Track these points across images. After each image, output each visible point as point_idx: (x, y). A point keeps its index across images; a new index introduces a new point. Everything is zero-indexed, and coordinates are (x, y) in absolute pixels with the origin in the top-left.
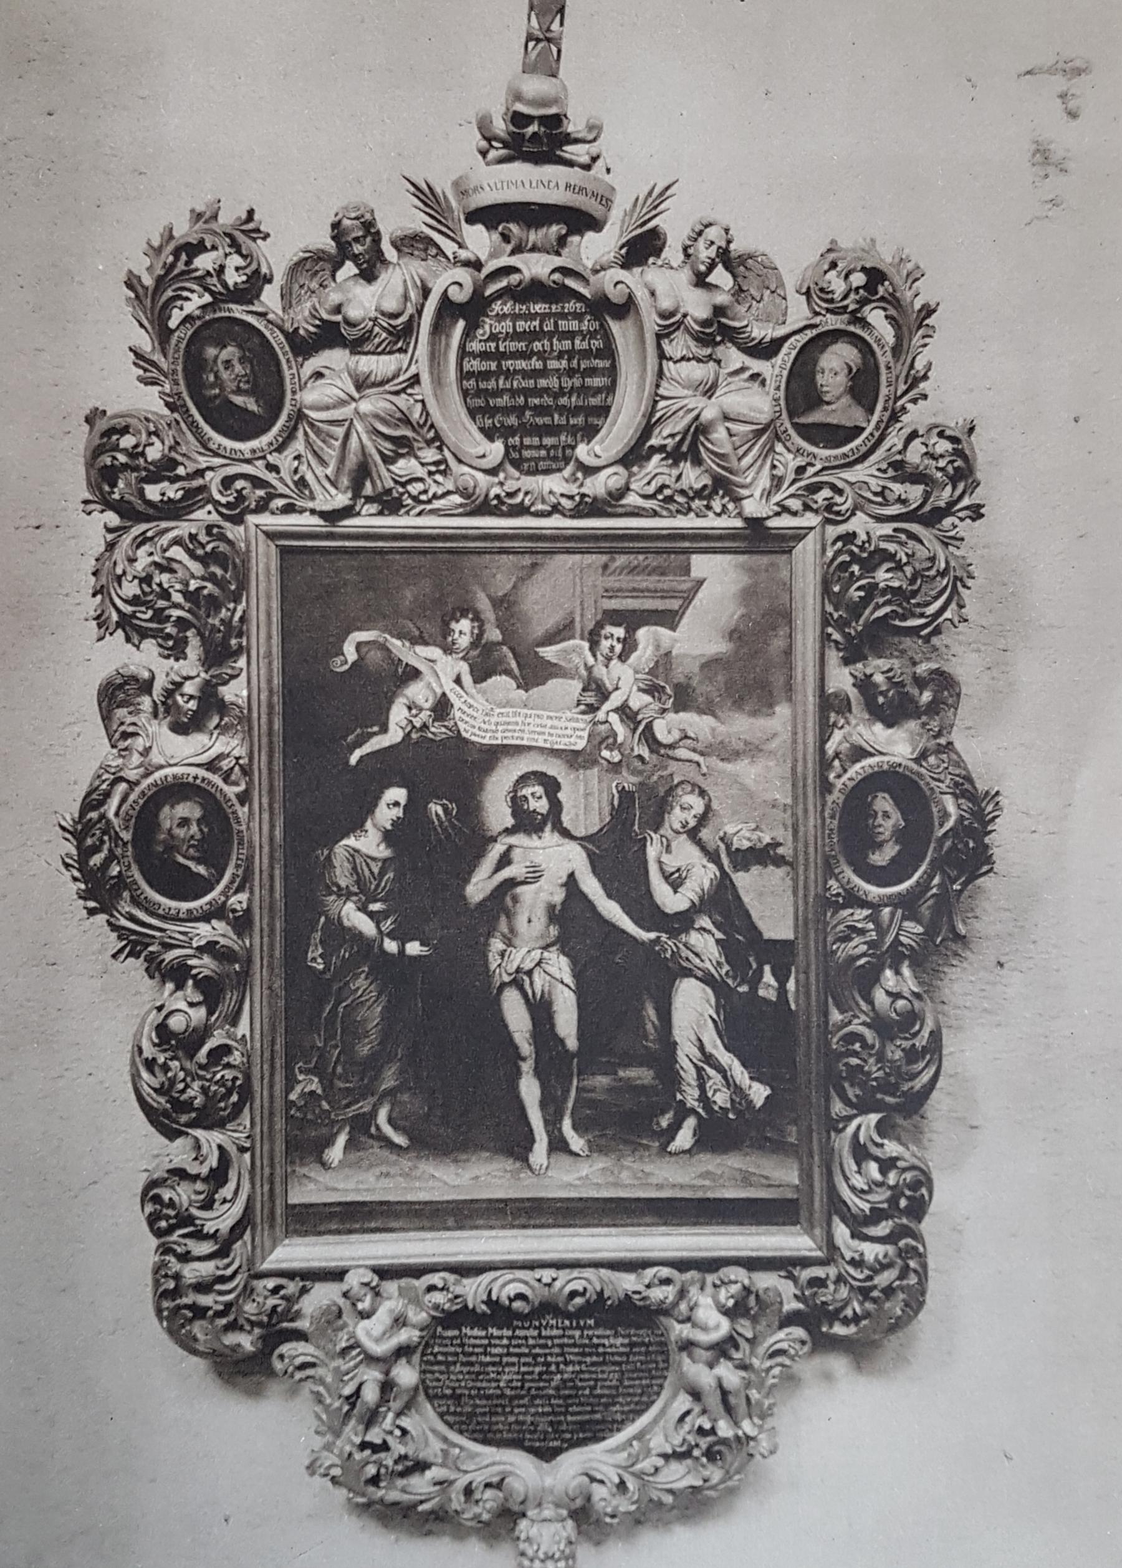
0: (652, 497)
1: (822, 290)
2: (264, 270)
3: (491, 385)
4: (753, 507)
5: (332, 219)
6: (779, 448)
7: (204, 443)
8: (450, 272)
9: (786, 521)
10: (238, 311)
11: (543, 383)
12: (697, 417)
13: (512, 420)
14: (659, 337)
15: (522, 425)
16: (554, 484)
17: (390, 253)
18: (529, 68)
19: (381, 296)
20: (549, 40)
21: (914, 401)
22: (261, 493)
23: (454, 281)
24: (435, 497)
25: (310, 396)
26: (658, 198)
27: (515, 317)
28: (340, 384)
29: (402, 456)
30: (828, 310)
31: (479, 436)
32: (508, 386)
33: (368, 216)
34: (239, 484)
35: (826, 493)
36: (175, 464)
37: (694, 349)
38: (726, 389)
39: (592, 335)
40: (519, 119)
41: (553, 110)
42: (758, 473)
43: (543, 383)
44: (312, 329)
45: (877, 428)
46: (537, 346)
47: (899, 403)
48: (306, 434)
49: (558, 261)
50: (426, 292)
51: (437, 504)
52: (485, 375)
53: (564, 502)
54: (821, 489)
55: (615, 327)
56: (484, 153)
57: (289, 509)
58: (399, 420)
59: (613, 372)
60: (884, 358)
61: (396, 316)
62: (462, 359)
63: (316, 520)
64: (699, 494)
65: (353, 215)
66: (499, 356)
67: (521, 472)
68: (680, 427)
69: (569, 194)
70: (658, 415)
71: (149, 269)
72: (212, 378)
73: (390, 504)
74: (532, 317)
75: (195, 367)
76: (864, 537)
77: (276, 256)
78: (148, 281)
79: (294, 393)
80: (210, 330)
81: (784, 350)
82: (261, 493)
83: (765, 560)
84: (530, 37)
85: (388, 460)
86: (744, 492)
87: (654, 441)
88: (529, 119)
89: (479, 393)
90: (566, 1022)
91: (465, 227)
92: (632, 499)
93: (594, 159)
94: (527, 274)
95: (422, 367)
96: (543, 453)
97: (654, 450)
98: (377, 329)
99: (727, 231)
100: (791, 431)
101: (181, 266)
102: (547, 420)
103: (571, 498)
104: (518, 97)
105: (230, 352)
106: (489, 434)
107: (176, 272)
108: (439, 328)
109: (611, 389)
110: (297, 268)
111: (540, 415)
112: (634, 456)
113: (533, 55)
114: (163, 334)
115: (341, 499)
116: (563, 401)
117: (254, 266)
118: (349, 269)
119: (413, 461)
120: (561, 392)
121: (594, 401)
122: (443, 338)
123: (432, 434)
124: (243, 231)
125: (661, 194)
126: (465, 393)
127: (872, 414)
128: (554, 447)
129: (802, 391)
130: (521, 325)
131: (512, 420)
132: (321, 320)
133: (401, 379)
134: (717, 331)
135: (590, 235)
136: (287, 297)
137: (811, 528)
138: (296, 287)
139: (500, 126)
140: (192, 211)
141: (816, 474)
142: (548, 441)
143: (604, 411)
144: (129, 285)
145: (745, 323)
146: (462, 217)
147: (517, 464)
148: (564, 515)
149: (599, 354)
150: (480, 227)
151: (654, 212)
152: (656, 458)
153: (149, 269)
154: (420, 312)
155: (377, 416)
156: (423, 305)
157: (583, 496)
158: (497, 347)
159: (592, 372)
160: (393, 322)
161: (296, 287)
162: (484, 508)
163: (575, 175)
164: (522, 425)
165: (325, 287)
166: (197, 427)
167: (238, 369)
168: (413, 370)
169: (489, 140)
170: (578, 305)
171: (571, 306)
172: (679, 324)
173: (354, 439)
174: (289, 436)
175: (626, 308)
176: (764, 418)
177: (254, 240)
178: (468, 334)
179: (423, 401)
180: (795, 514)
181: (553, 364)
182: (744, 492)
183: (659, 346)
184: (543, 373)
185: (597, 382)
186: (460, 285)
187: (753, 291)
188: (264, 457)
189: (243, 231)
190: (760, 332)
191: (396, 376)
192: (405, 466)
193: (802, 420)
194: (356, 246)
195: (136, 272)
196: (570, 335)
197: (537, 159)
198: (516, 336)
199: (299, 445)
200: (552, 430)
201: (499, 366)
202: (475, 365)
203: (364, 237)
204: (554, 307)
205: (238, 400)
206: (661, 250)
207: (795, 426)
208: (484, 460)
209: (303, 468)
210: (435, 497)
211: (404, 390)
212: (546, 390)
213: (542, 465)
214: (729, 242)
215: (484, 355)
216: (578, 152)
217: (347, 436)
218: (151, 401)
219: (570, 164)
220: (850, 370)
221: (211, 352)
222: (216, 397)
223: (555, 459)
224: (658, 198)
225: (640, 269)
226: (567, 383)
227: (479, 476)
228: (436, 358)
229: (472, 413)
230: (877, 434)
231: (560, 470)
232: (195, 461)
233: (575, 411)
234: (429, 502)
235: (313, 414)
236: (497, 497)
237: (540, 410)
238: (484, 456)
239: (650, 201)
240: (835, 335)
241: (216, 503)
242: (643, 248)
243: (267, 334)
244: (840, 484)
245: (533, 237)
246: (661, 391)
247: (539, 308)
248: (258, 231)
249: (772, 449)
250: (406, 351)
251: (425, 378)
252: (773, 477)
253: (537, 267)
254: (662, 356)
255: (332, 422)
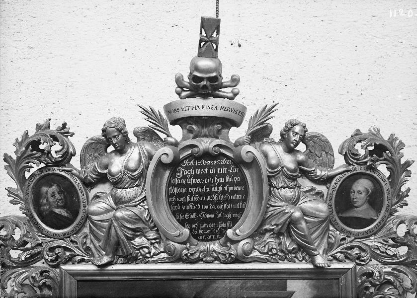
0: (267, 253)
1: (353, 154)
2: (71, 150)
3: (183, 200)
4: (320, 260)
5: (102, 127)
6: (331, 228)
7: (40, 230)
8: (164, 148)
9: (335, 265)
10: (57, 170)
11: (210, 198)
12: (290, 217)
13: (194, 216)
14: (269, 177)
15: (199, 218)
16: (215, 246)
17: (133, 139)
18: (200, 55)
19: (128, 161)
20: (212, 42)
21: (402, 207)
22: (68, 254)
23: (165, 153)
24: (155, 254)
25: (93, 208)
26: (267, 112)
27: (195, 168)
28: (107, 202)
29: (137, 236)
30: (356, 163)
31: (177, 224)
32: (192, 200)
33: (120, 126)
34: (57, 251)
35: (356, 251)
36: (26, 243)
37: (287, 183)
38: (304, 200)
39: (235, 175)
40: (195, 79)
41: (214, 74)
42: (321, 241)
43: (210, 198)
44: (94, 176)
45: (382, 220)
46: (207, 181)
47: (393, 207)
48: (90, 225)
49: (218, 142)
50: (150, 157)
51: (155, 258)
52: (180, 195)
53: (220, 256)
54: (353, 248)
55: (246, 172)
56: (179, 94)
57: (82, 261)
58: (136, 219)
59: (246, 192)
60: (386, 187)
61: (135, 170)
62: (169, 187)
63: (94, 268)
64: (291, 252)
65: (113, 125)
66: (187, 186)
67: (199, 240)
68: (282, 220)
69: (222, 111)
70: (269, 214)
71: (16, 152)
72: (45, 201)
73: (130, 259)
74: (203, 167)
75: (37, 197)
76: (377, 274)
77: (78, 143)
78: (15, 157)
79: (85, 206)
80: (45, 179)
81: (334, 181)
82: (68, 254)
83: (325, 283)
84: (201, 41)
85: (129, 239)
86: (315, 253)
87: (267, 227)
88: (201, 79)
89: (177, 203)
90: (272, 233)
91: (170, 127)
92: (255, 254)
93: (236, 95)
94: (201, 148)
95: (148, 193)
96: (210, 231)
97: (267, 231)
98: (125, 177)
99: (304, 127)
100: (337, 219)
101: (29, 153)
102: (212, 216)
103: (225, 255)
104: (197, 69)
105: (54, 189)
106: (183, 223)
107: (26, 155)
108: (157, 174)
109: (245, 201)
110: (87, 148)
111: (209, 213)
112: (258, 233)
113: (203, 49)
114: (21, 180)
115: (105, 260)
116: (220, 207)
117: (65, 150)
118: (111, 149)
119: (143, 238)
120: (219, 202)
121: (238, 206)
122: (159, 179)
123: (152, 225)
124: (61, 133)
125: (268, 111)
126: (170, 204)
127: (380, 212)
128: (216, 228)
129: (343, 200)
130: (198, 171)
131: (194, 216)
132: (98, 172)
133: (139, 199)
134: (301, 170)
135: (233, 128)
136: (83, 161)
137: (349, 269)
138: (88, 156)
139: (186, 80)
140: (37, 125)
141: (351, 242)
142: (212, 226)
143: (241, 211)
144: (5, 160)
145: (314, 169)
146: (168, 123)
147: (196, 237)
148: (221, 263)
149: (238, 184)
150: (178, 127)
151: (266, 118)
152: (267, 235)
153: (16, 152)
154: (147, 168)
155: (124, 219)
156: (149, 164)
157: (230, 254)
158: (186, 182)
159: (235, 192)
160: (134, 174)
161: (88, 156)
162: (179, 260)
163: (225, 102)
164: (199, 218)
165: (101, 156)
166: (37, 224)
167: (58, 196)
168: (144, 195)
169: (182, 88)
170: (228, 161)
171: (223, 161)
172: (278, 172)
173: (113, 230)
174: (82, 225)
175: (253, 164)
176: (324, 215)
177: (67, 136)
178: (172, 176)
179: (148, 209)
180: (340, 261)
181: (215, 189)
182: (315, 253)
183: (269, 181)
184: (210, 193)
185: (238, 197)
186: (167, 154)
187: (317, 153)
188: (69, 237)
189: (61, 133)
190: (321, 173)
191: (135, 197)
192: (138, 241)
193: (344, 215)
194: (113, 139)
195: (9, 154)
196: (223, 175)
197: (204, 96)
198: (196, 176)
199: (86, 230)
200: (215, 220)
201: (187, 190)
202: (176, 191)
203: (119, 135)
204: (215, 162)
205: (57, 211)
206: (269, 134)
207: (339, 217)
208: (181, 237)
209: (88, 241)
210: (155, 254)
211: (139, 204)
212: (212, 202)
213: (210, 237)
214: (305, 131)
215: (180, 186)
216: (227, 91)
217: (110, 228)
218: (16, 211)
219: (223, 97)
220: (368, 191)
221: (44, 189)
222: (47, 210)
223: (216, 234)
224: (267, 112)
225: (259, 143)
226: (222, 197)
227: (177, 245)
228: (155, 191)
229: (174, 213)
230: (382, 223)
231: (218, 239)
232: (38, 240)
233: (227, 211)
234: (151, 257)
235: (94, 218)
236: (186, 255)
237: (208, 211)
238: (179, 236)
239: (263, 114)
240: (360, 175)
241: (46, 260)
242: (260, 134)
243: (72, 180)
244: (364, 247)
245: (205, 131)
246: (270, 203)
247: (208, 163)
248: (68, 133)
249: (328, 229)
250: (140, 186)
251: (150, 199)
252: (329, 243)
253: (206, 144)
254: (271, 185)
255: (102, 221)
